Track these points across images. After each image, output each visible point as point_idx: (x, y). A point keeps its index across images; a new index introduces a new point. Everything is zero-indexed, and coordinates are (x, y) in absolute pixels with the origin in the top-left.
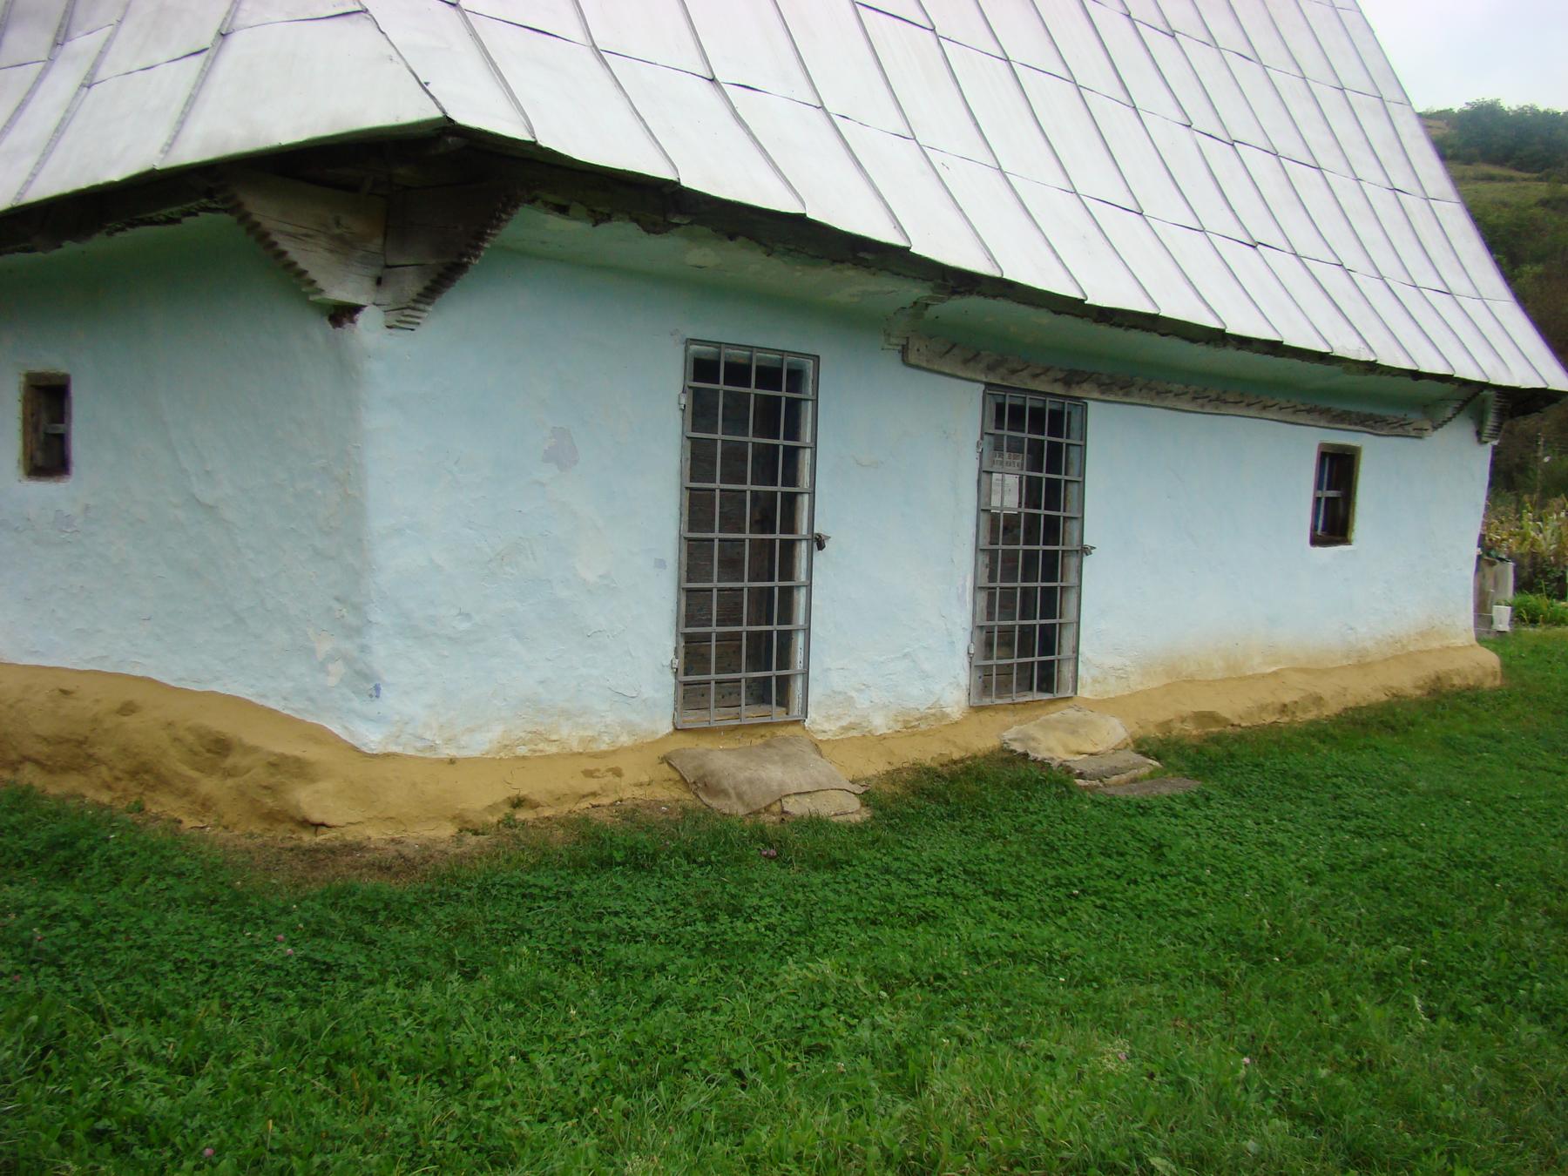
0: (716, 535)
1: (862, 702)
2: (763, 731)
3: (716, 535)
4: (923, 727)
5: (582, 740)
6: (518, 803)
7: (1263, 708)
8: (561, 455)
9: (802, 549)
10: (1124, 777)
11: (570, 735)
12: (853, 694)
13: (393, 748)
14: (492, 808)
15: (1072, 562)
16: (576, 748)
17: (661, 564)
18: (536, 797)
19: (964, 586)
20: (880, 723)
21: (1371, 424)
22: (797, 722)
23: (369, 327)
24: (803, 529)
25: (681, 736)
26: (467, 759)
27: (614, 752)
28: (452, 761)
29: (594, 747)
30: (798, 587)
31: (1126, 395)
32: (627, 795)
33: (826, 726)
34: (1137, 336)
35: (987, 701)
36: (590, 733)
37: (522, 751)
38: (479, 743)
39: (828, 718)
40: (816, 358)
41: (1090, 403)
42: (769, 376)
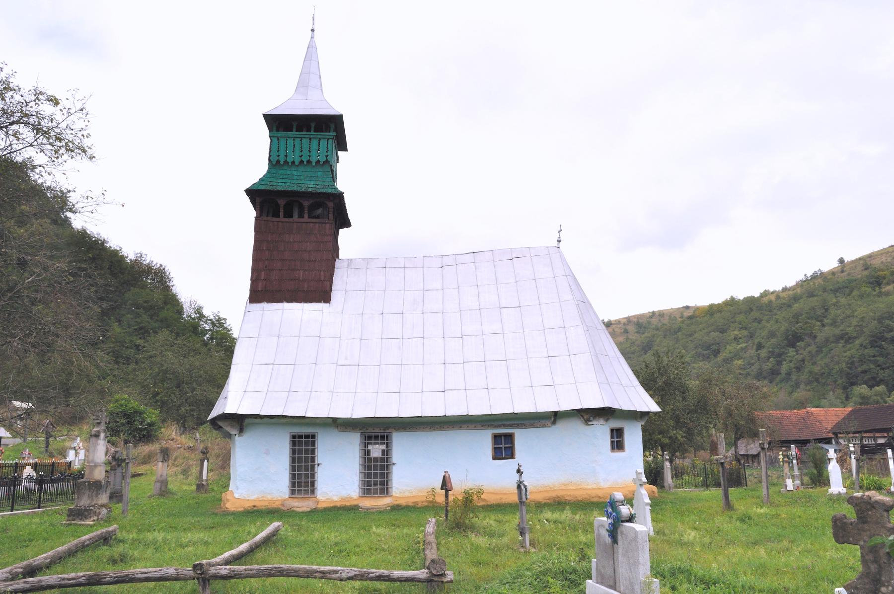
4: (346, 500)
6: (254, 506)
8: (267, 453)
9: (316, 466)
11: (269, 497)
12: (328, 493)
14: (249, 507)
15: (391, 467)
16: (270, 499)
18: (258, 506)
20: (335, 498)
21: (518, 426)
23: (237, 438)
24: (316, 462)
28: (248, 500)
29: (274, 499)
31: (405, 430)
34: (385, 419)
35: (293, 496)
37: (260, 499)
38: (254, 497)
39: (323, 497)
42: (307, 437)
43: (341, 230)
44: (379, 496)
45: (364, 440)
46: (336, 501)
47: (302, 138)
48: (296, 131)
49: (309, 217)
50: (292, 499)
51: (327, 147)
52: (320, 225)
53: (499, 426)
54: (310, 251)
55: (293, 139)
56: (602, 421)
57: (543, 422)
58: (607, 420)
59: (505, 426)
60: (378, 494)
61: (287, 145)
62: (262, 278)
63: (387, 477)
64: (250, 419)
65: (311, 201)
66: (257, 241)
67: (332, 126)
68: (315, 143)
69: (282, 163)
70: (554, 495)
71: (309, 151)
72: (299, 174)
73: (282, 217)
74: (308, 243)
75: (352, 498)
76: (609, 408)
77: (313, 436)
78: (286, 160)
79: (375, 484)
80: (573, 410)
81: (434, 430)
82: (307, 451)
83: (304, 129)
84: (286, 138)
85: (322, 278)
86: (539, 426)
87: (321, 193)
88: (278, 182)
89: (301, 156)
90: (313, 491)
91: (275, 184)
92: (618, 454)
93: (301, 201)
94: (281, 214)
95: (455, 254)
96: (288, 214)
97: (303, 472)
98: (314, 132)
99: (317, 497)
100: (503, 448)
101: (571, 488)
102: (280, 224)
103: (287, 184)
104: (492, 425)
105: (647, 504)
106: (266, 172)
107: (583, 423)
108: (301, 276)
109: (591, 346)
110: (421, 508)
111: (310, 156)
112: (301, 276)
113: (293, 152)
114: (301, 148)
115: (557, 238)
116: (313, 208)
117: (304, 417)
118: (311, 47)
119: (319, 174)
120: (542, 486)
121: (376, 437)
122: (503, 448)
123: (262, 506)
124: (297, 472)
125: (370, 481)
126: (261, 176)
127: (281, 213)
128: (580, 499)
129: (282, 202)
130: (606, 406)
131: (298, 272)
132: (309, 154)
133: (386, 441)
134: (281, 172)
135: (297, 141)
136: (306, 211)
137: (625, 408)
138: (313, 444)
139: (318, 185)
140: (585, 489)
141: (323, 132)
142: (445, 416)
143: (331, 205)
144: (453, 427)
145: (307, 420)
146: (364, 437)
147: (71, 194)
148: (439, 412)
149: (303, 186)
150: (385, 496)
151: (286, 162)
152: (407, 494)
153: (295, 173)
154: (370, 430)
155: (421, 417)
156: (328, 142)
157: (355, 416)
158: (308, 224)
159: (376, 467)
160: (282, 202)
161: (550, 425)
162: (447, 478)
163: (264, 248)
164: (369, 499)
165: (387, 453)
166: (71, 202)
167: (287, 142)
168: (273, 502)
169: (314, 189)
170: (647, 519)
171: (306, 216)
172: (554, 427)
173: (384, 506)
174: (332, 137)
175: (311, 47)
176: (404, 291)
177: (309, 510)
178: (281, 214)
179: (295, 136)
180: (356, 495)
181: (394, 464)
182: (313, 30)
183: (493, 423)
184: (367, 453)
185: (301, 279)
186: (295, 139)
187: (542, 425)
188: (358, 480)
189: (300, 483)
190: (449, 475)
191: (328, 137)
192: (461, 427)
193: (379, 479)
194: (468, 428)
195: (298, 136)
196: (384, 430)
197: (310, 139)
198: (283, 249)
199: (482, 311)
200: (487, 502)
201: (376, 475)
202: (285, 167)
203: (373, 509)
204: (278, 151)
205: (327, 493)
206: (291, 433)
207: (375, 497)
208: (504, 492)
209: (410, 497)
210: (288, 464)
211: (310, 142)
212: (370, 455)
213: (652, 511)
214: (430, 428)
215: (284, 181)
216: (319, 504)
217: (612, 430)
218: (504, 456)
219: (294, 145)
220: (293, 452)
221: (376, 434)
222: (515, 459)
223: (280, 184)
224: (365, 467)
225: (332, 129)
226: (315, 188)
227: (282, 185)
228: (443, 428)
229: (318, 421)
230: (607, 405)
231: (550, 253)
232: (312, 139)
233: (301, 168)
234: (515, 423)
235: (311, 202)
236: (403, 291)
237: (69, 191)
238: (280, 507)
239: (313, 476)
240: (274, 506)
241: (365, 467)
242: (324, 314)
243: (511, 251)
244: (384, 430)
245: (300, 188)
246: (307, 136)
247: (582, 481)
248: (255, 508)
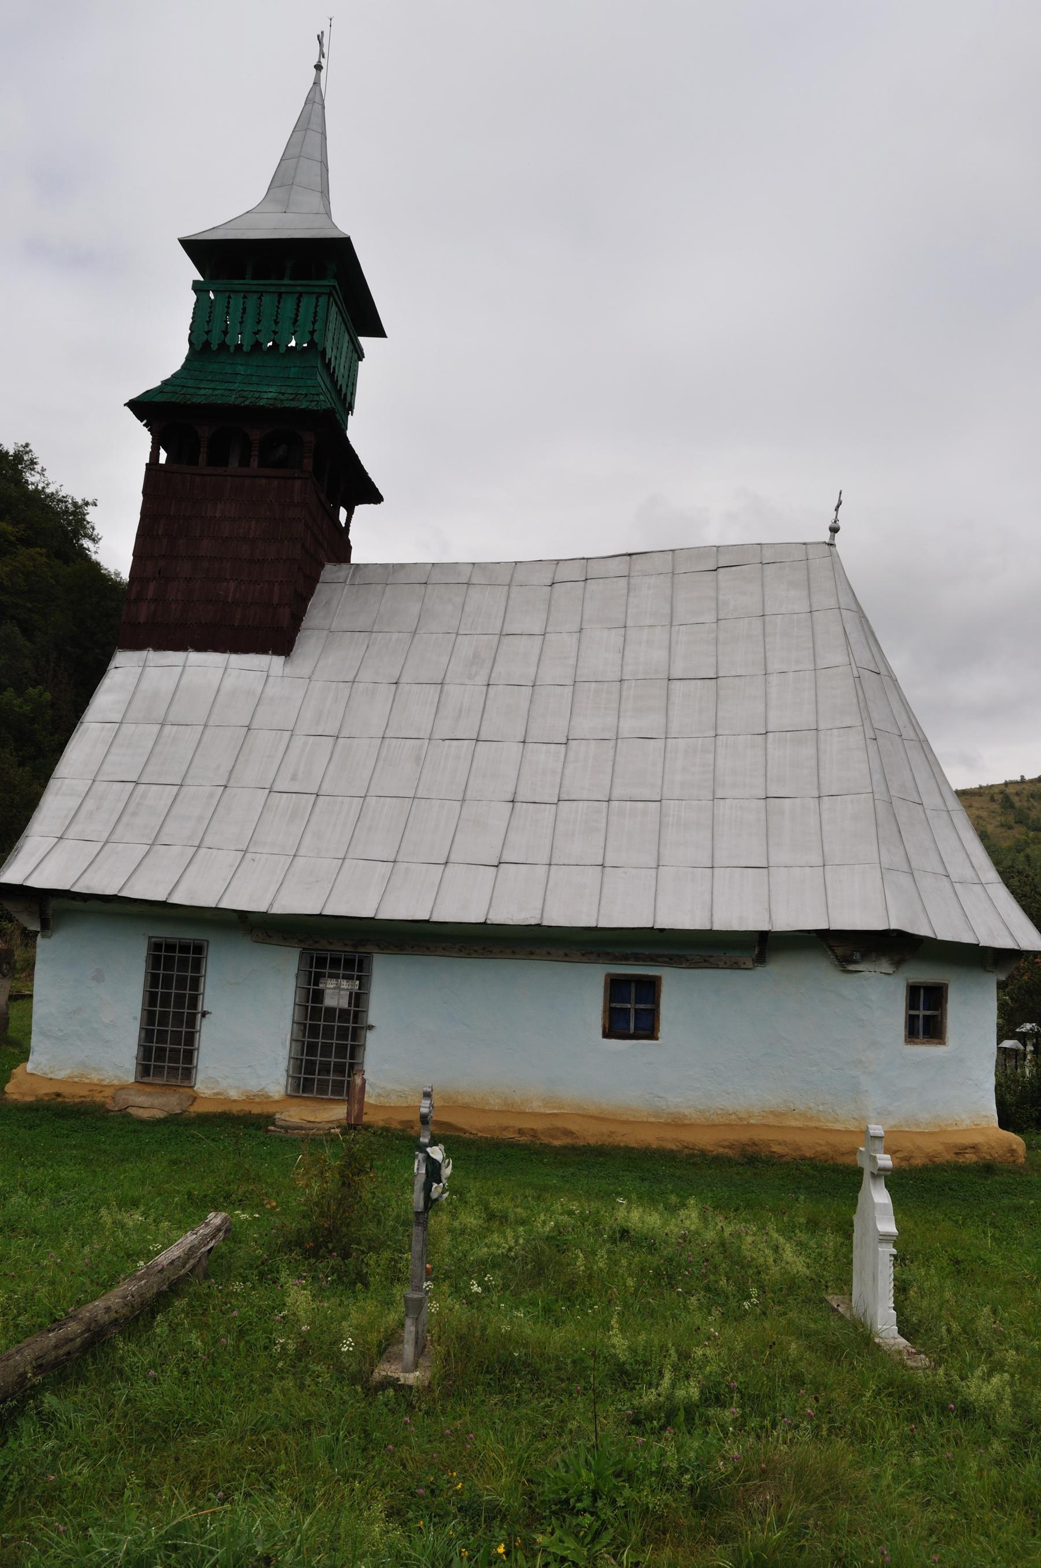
3: (186, 1011)
4: (257, 1100)
5: (99, 1079)
6: (58, 1095)
8: (99, 978)
9: (199, 1016)
11: (95, 1077)
12: (219, 1079)
13: (34, 1072)
14: (46, 1094)
16: (96, 1081)
17: (135, 1018)
19: (286, 1039)
20: (234, 1094)
24: (200, 1009)
25: (137, 1084)
27: (109, 1086)
28: (51, 1079)
31: (402, 950)
33: (206, 1091)
35: (146, 1080)
36: (102, 1077)
37: (76, 1080)
38: (61, 1075)
39: (207, 1088)
40: (208, 941)
42: (184, 948)
46: (235, 1101)
48: (254, 278)
50: (141, 1087)
51: (315, 313)
53: (624, 959)
55: (242, 295)
60: (327, 1095)
61: (228, 307)
63: (352, 1057)
69: (214, 347)
70: (744, 1136)
71: (276, 322)
72: (248, 373)
75: (269, 1097)
76: (900, 934)
77: (199, 949)
79: (325, 1069)
81: (469, 956)
82: (181, 983)
84: (227, 294)
86: (721, 964)
88: (200, 388)
89: (256, 333)
94: (203, 458)
98: (291, 279)
100: (632, 1013)
101: (793, 1123)
103: (217, 392)
104: (608, 954)
105: (885, 1238)
106: (180, 368)
107: (836, 965)
108: (231, 595)
109: (877, 777)
110: (528, 1113)
111: (275, 333)
112: (231, 595)
113: (241, 323)
114: (259, 314)
115: (829, 523)
118: (315, 100)
120: (720, 1112)
121: (335, 963)
122: (632, 1013)
123: (73, 1096)
124: (156, 1027)
125: (313, 1063)
127: (201, 458)
128: (808, 1155)
130: (893, 927)
132: (274, 327)
137: (944, 935)
138: (197, 966)
141: (311, 279)
147: (90, 509)
148: (584, 918)
150: (330, 1100)
151: (223, 346)
153: (241, 369)
159: (328, 1032)
161: (750, 964)
162: (357, 1089)
164: (308, 1103)
165: (359, 999)
166: (88, 523)
167: (229, 303)
168: (100, 1089)
170: (880, 1283)
171: (255, 463)
172: (760, 970)
173: (327, 1126)
174: (326, 290)
175: (315, 100)
176: (457, 634)
178: (203, 458)
180: (279, 1092)
182: (318, 67)
184: (318, 996)
188: (287, 1057)
192: (532, 953)
193: (333, 1059)
194: (549, 957)
195: (253, 288)
196: (355, 946)
199: (626, 684)
200: (578, 1138)
201: (326, 1050)
203: (301, 1128)
204: (208, 322)
205: (217, 1081)
206: (150, 938)
207: (322, 1099)
208: (625, 1117)
210: (140, 1007)
211: (279, 302)
213: (899, 1260)
214: (461, 951)
215: (212, 385)
216: (195, 1103)
219: (244, 309)
222: (657, 1039)
223: (202, 392)
227: (206, 393)
228: (491, 952)
230: (894, 926)
231: (810, 557)
232: (283, 295)
234: (666, 952)
236: (454, 636)
237: (87, 504)
238: (108, 1101)
240: (98, 1098)
242: (270, 679)
246: (273, 289)
247: (821, 1108)
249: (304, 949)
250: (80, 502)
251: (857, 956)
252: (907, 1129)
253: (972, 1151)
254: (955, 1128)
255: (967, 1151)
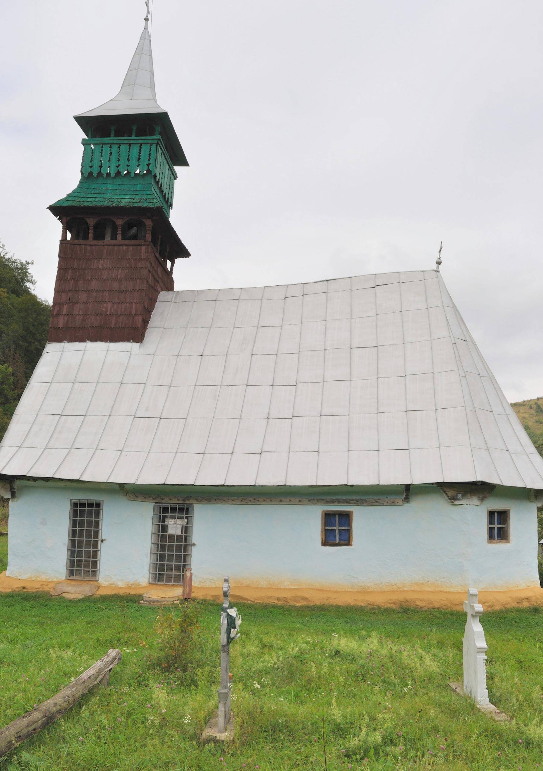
0: (92, 539)
1: (132, 582)
2: (88, 582)
4: (133, 587)
6: (24, 588)
7: (270, 597)
9: (100, 542)
10: (159, 603)
11: (44, 577)
13: (10, 576)
14: (17, 588)
15: (190, 548)
16: (44, 580)
17: (65, 544)
18: (27, 587)
20: (120, 584)
21: (358, 502)
22: (97, 581)
24: (100, 538)
25: (67, 580)
26: (23, 579)
28: (19, 579)
30: (99, 551)
31: (209, 501)
32: (46, 590)
33: (105, 583)
35: (72, 578)
36: (47, 577)
37: (33, 579)
38: (25, 577)
41: (195, 505)
42: (90, 505)
43: (176, 260)
44: (173, 585)
45: (159, 512)
46: (121, 588)
47: (120, 144)
48: (115, 136)
49: (123, 238)
51: (150, 154)
52: (135, 247)
53: (332, 502)
54: (121, 280)
55: (109, 146)
56: (475, 501)
57: (392, 498)
58: (482, 499)
59: (339, 502)
61: (102, 153)
62: (64, 313)
64: (22, 481)
65: (126, 219)
66: (61, 268)
67: (158, 129)
68: (135, 150)
69: (95, 175)
70: (401, 597)
71: (128, 160)
72: (114, 188)
73: (91, 239)
74: (120, 270)
75: (139, 585)
76: (483, 483)
77: (98, 505)
78: (100, 171)
79: (170, 568)
80: (433, 484)
81: (247, 503)
82: (89, 524)
83: (125, 135)
84: (101, 146)
85: (133, 312)
86: (385, 503)
87: (135, 207)
90: (94, 573)
91: (83, 199)
92: (499, 547)
93: (114, 220)
94: (91, 235)
95: (303, 283)
96: (99, 236)
97: (84, 549)
98: (136, 136)
99: (99, 582)
101: (428, 589)
102: (88, 247)
104: (323, 500)
105: (480, 650)
106: (76, 187)
108: (109, 310)
111: (128, 166)
112: (109, 310)
115: (436, 259)
116: (128, 226)
117: (78, 481)
119: (139, 187)
120: (387, 584)
121: (173, 510)
124: (76, 549)
126: (70, 192)
128: (436, 606)
129: (91, 222)
131: (105, 305)
132: (127, 163)
133: (185, 515)
134: (95, 186)
135: (115, 148)
136: (119, 232)
138: (98, 514)
139: (134, 199)
140: (446, 592)
141: (147, 136)
142: (255, 485)
143: (149, 223)
144: (271, 501)
145: (83, 485)
146: (159, 508)
147: (30, 266)
149: (115, 200)
151: (100, 174)
152: (208, 585)
153: (110, 187)
154: (167, 500)
155: (223, 486)
156: (151, 148)
157: (141, 482)
158: (121, 247)
159: (171, 548)
160: (91, 222)
161: (401, 502)
162: (188, 579)
163: (69, 278)
165: (186, 529)
166: (29, 274)
167: (102, 150)
168: (46, 584)
169: (127, 204)
171: (119, 237)
172: (406, 506)
174: (156, 141)
176: (234, 327)
177: (80, 597)
178: (91, 235)
179: (111, 142)
181: (194, 545)
182: (147, 19)
183: (324, 498)
184: (164, 528)
185: (108, 313)
186: (112, 146)
187: (389, 503)
189: (79, 562)
190: (191, 574)
191: (150, 141)
192: (281, 501)
193: (174, 563)
194: (290, 502)
195: (115, 142)
196: (184, 500)
197: (130, 145)
198: (89, 278)
199: (327, 352)
200: (310, 601)
201: (170, 557)
202: (100, 180)
203: (158, 601)
206: (71, 500)
207: (169, 585)
209: (212, 588)
211: (130, 149)
212: (167, 532)
215: (95, 196)
216: (99, 590)
217: (491, 514)
218: (337, 541)
219: (111, 154)
220: (74, 523)
221: (174, 506)
222: (351, 545)
223: (89, 200)
224: (158, 546)
225: (157, 132)
226: (129, 202)
227: (91, 201)
229: (102, 486)
230: (479, 479)
232: (132, 145)
233: (118, 181)
234: (354, 498)
235: (126, 220)
236: (232, 328)
237: (28, 263)
239: (95, 554)
241: (158, 546)
243: (375, 276)
244: (184, 500)
245: (111, 203)
246: (126, 142)
247: (443, 580)
248: (25, 590)
249: (156, 503)
250: (24, 263)
251: (460, 496)
252: (490, 590)
253: (527, 600)
254: (517, 589)
255: (524, 601)
